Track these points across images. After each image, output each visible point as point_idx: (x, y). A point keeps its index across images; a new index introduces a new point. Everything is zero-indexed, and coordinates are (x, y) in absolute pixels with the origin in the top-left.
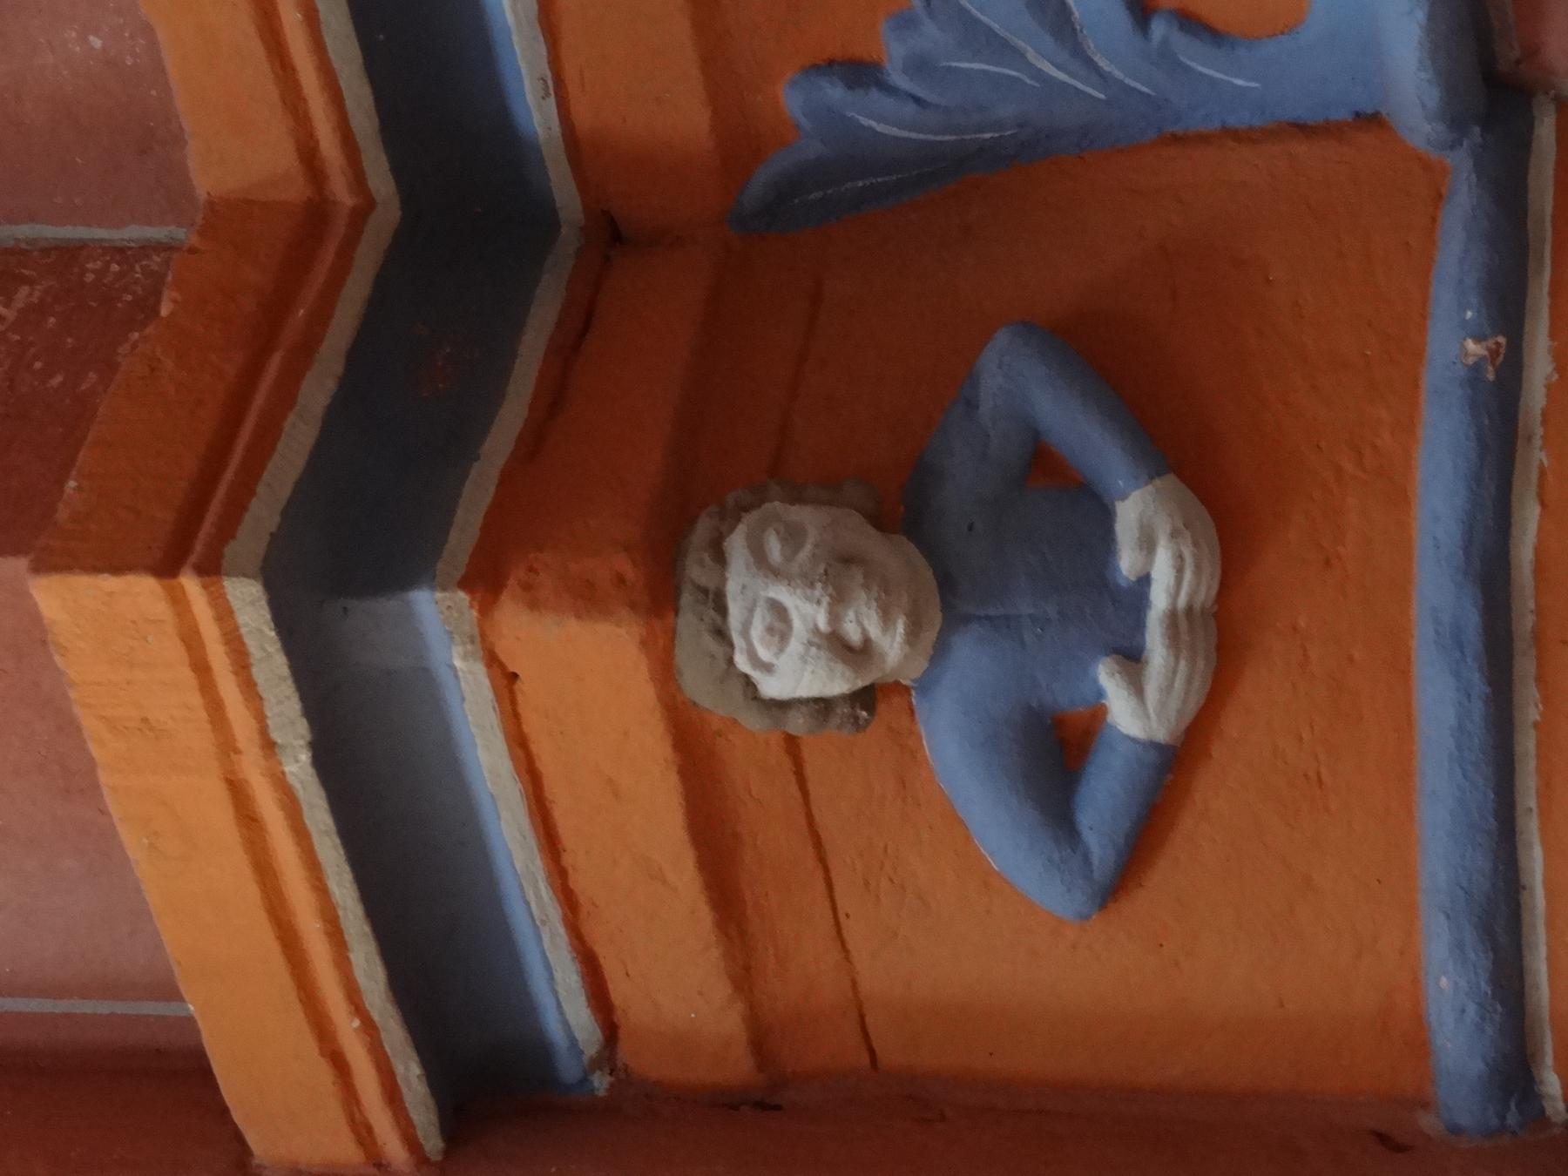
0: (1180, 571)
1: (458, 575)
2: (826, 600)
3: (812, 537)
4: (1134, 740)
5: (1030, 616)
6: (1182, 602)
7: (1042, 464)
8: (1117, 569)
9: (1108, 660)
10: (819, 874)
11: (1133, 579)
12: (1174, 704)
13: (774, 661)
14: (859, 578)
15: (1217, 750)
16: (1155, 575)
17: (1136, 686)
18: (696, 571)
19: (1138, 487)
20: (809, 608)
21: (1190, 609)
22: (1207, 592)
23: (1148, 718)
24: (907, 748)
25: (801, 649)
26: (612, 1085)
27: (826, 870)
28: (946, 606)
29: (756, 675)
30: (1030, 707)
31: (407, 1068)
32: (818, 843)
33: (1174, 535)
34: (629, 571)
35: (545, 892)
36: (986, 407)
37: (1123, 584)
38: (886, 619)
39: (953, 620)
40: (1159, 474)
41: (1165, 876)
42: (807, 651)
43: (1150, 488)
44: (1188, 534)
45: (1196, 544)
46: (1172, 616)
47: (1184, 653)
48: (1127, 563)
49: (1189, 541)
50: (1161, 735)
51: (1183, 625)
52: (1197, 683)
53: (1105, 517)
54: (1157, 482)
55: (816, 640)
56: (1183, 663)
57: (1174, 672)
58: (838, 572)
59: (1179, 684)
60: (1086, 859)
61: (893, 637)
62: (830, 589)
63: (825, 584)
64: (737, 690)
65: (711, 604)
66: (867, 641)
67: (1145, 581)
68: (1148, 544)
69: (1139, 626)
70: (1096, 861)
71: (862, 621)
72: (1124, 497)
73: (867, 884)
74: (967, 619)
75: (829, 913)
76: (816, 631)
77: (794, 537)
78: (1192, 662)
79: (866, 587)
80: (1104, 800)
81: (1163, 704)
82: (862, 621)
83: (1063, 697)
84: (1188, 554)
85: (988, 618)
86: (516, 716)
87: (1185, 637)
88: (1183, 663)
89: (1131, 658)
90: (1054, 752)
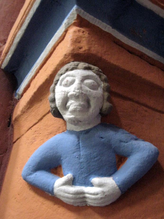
0: (94, 194)
1: (81, 15)
2: (75, 93)
3: (94, 92)
4: (54, 184)
5: (80, 155)
6: (87, 195)
7: (121, 158)
8: (94, 177)
9: (72, 176)
10: (36, 121)
11: (92, 181)
12: (62, 194)
13: (62, 85)
14: (82, 103)
15: (56, 206)
16: (93, 188)
17: (66, 183)
18: (82, 65)
19: (116, 182)
20: (73, 90)
21: (85, 197)
22: (90, 202)
23: (58, 187)
24: (57, 131)
25: (64, 90)
26: (16, 99)
27: (38, 122)
28: (81, 132)
29: (59, 82)
30: (61, 158)
31: (10, 55)
32: (41, 119)
33: (103, 192)
34: (83, 49)
35: (35, 70)
36: (134, 142)
37: (90, 179)
38: (74, 112)
39: (78, 135)
40: (120, 188)
41: (31, 194)
42: (63, 92)
43: (116, 186)
44: (104, 196)
45: (101, 198)
46: (83, 193)
47: (74, 196)
48: (95, 180)
49: (102, 196)
50: (55, 191)
51: (81, 196)
52: (67, 200)
53: (109, 175)
54: (118, 188)
55: (66, 93)
56: (71, 196)
57: (69, 193)
58: (85, 99)
59: (66, 195)
60: (30, 174)
61: (69, 115)
62: (77, 94)
63: (79, 92)
64: (56, 82)
65: (74, 66)
66: (68, 108)
67: (92, 185)
68: (100, 185)
69: (81, 184)
70: (30, 177)
71: (72, 104)
72: (113, 179)
73: (36, 131)
74: (78, 137)
75: (32, 125)
76: (68, 93)
77: (93, 87)
78: (72, 198)
79: (80, 105)
80: (43, 177)
81: (61, 191)
82: (72, 104)
83: (65, 165)
84: (99, 196)
85: (79, 143)
86: (58, 45)
87: (78, 196)
88: (71, 196)
89: (72, 182)
90: (51, 164)
